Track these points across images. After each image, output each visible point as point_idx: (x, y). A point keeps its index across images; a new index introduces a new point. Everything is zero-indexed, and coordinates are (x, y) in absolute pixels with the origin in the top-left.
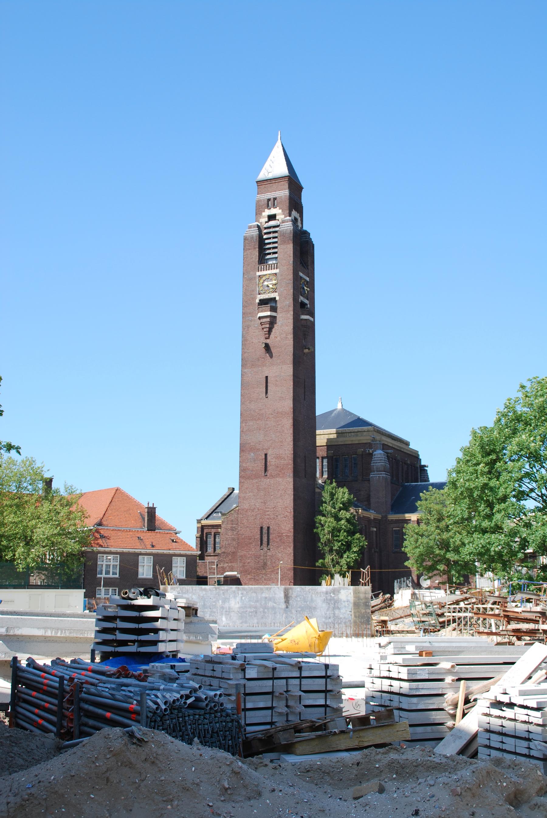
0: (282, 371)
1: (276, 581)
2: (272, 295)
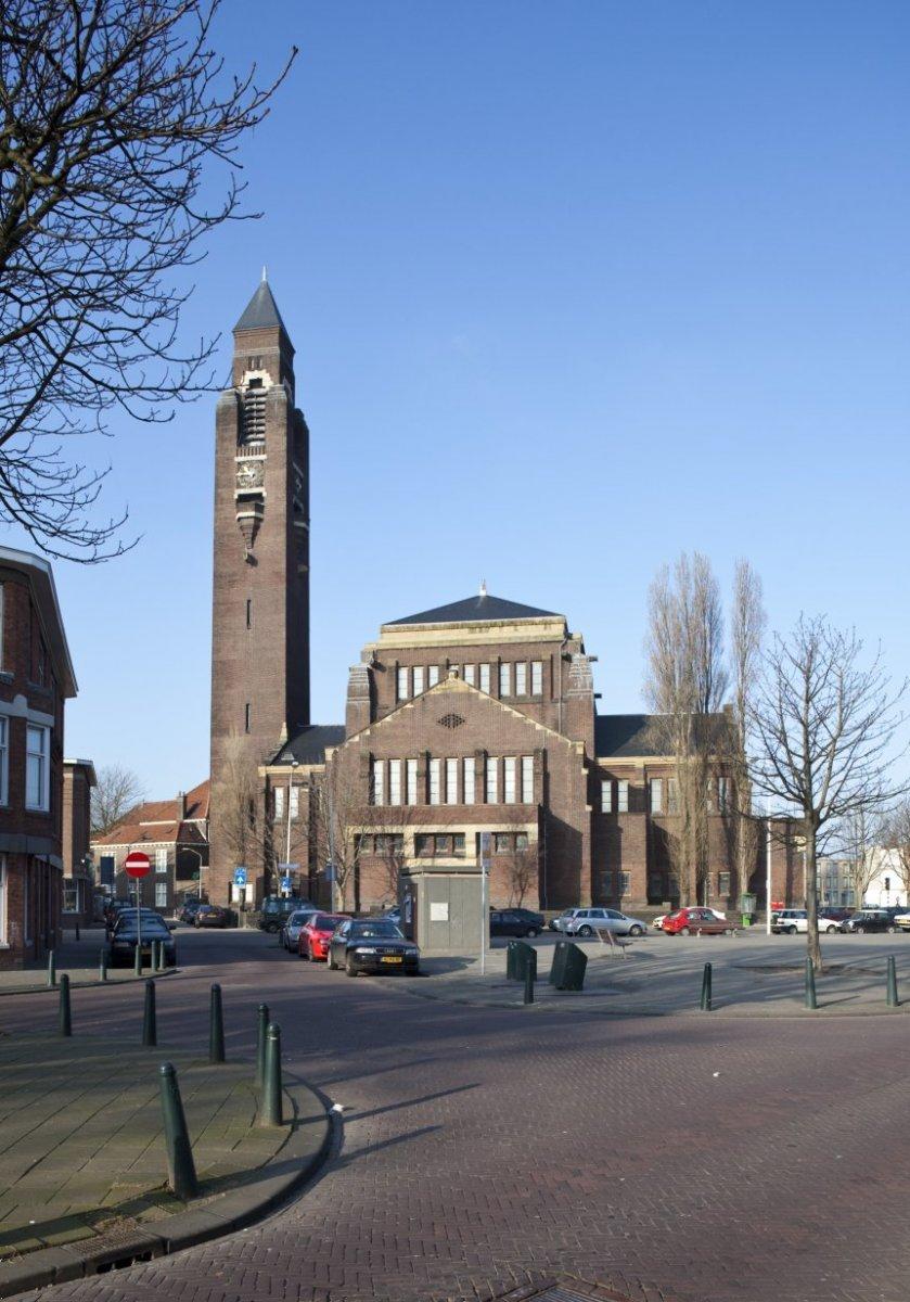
2: (256, 490)
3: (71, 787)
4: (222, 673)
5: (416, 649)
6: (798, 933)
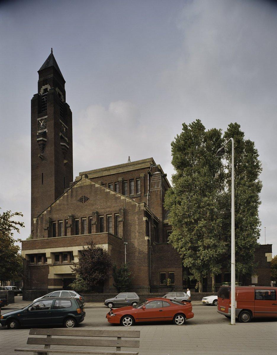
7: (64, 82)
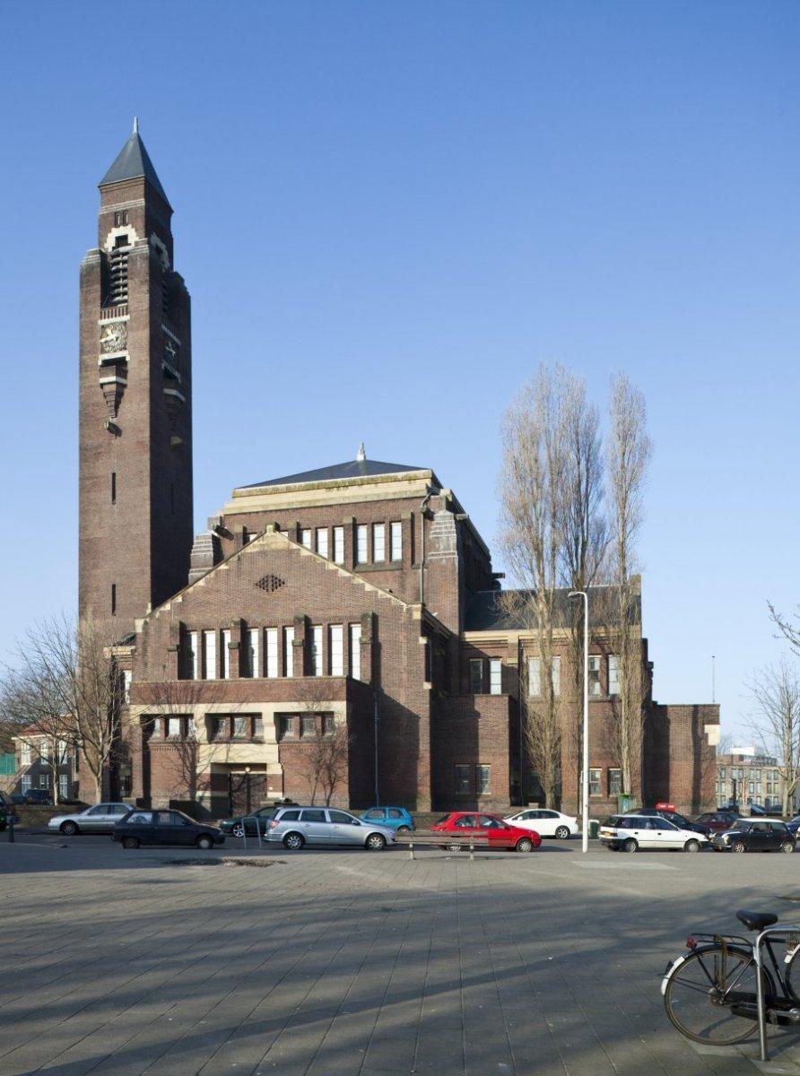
0: (132, 461)
1: (262, 779)
2: (119, 355)
3: (428, 748)
4: (88, 550)
5: (265, 512)
6: (639, 850)
7: (169, 211)
